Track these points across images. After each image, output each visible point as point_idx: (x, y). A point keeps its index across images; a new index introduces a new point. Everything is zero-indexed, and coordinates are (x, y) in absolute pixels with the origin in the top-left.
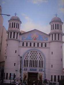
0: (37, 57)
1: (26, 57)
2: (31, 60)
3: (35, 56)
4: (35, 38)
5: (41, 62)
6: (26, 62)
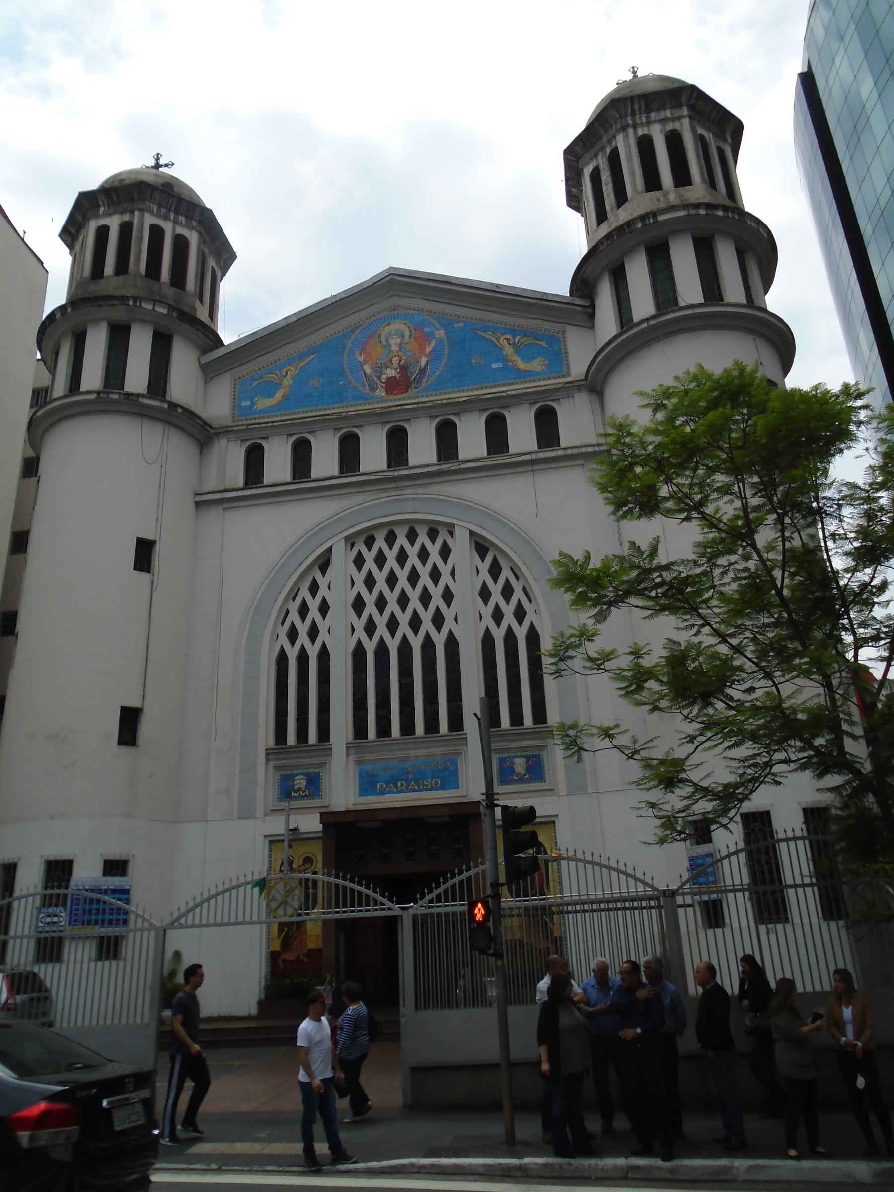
0: (448, 596)
1: (304, 610)
2: (370, 647)
4: (403, 369)
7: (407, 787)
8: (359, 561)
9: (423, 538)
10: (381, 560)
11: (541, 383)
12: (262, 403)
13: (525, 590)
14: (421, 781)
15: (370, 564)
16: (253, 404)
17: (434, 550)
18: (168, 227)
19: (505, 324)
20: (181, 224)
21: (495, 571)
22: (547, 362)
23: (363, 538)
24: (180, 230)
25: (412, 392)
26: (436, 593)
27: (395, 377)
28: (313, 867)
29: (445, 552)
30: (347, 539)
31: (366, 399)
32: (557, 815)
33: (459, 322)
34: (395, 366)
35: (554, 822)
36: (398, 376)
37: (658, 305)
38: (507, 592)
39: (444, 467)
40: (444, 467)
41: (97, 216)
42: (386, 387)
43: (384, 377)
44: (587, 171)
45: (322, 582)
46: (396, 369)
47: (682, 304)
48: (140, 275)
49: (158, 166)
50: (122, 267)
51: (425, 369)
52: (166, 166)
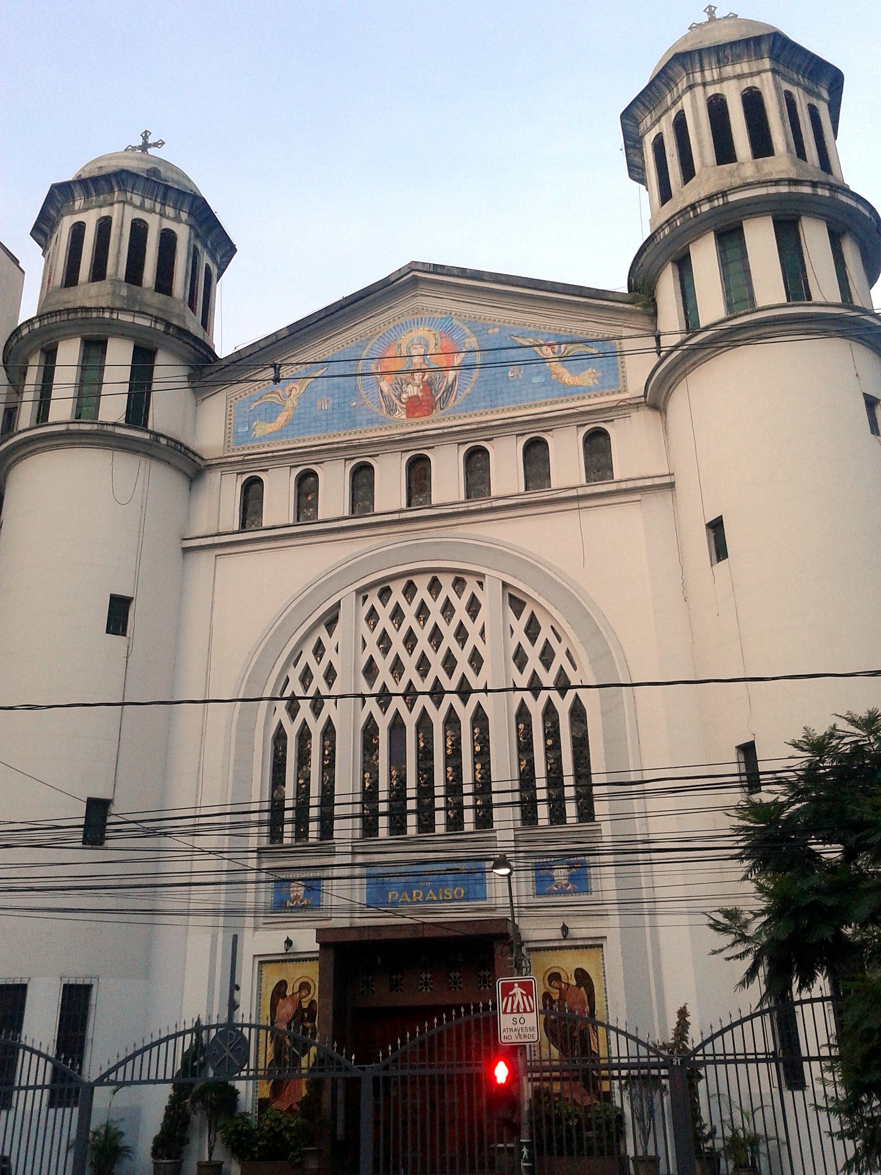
3: (423, 644)
4: (428, 386)
5: (552, 733)
6: (303, 758)
7: (424, 897)
8: (372, 616)
9: (447, 591)
10: (397, 615)
11: (591, 401)
12: (262, 429)
13: (568, 653)
14: (441, 890)
15: (385, 622)
16: (251, 430)
17: (460, 604)
18: (154, 226)
19: (550, 329)
20: (168, 218)
21: (532, 630)
22: (599, 374)
23: (377, 590)
24: (168, 224)
25: (436, 414)
26: (462, 656)
27: (417, 396)
28: (310, 996)
29: (474, 607)
30: (358, 592)
31: (384, 423)
32: (606, 937)
33: (494, 327)
34: (417, 382)
35: (601, 946)
36: (420, 394)
37: (729, 306)
38: (547, 656)
39: (474, 506)
40: (474, 506)
41: (73, 213)
42: (407, 408)
43: (404, 396)
44: (649, 140)
45: (329, 643)
46: (419, 386)
47: (760, 303)
48: (120, 281)
49: (145, 146)
50: (98, 272)
51: (452, 386)
52: (155, 145)
